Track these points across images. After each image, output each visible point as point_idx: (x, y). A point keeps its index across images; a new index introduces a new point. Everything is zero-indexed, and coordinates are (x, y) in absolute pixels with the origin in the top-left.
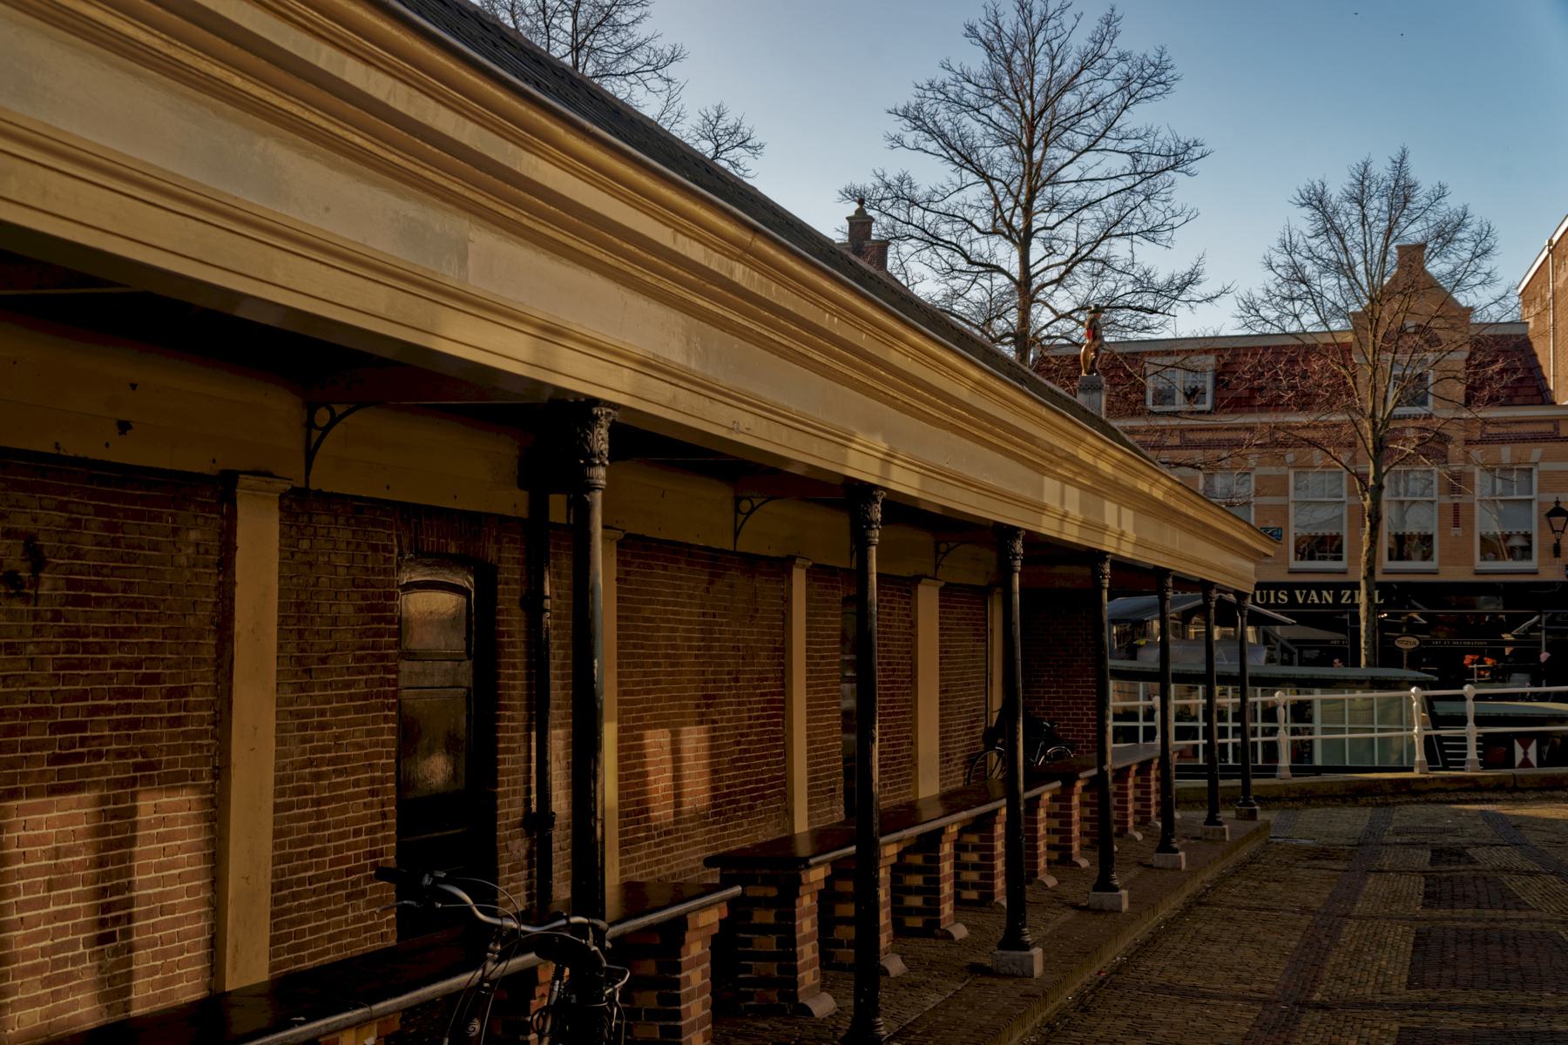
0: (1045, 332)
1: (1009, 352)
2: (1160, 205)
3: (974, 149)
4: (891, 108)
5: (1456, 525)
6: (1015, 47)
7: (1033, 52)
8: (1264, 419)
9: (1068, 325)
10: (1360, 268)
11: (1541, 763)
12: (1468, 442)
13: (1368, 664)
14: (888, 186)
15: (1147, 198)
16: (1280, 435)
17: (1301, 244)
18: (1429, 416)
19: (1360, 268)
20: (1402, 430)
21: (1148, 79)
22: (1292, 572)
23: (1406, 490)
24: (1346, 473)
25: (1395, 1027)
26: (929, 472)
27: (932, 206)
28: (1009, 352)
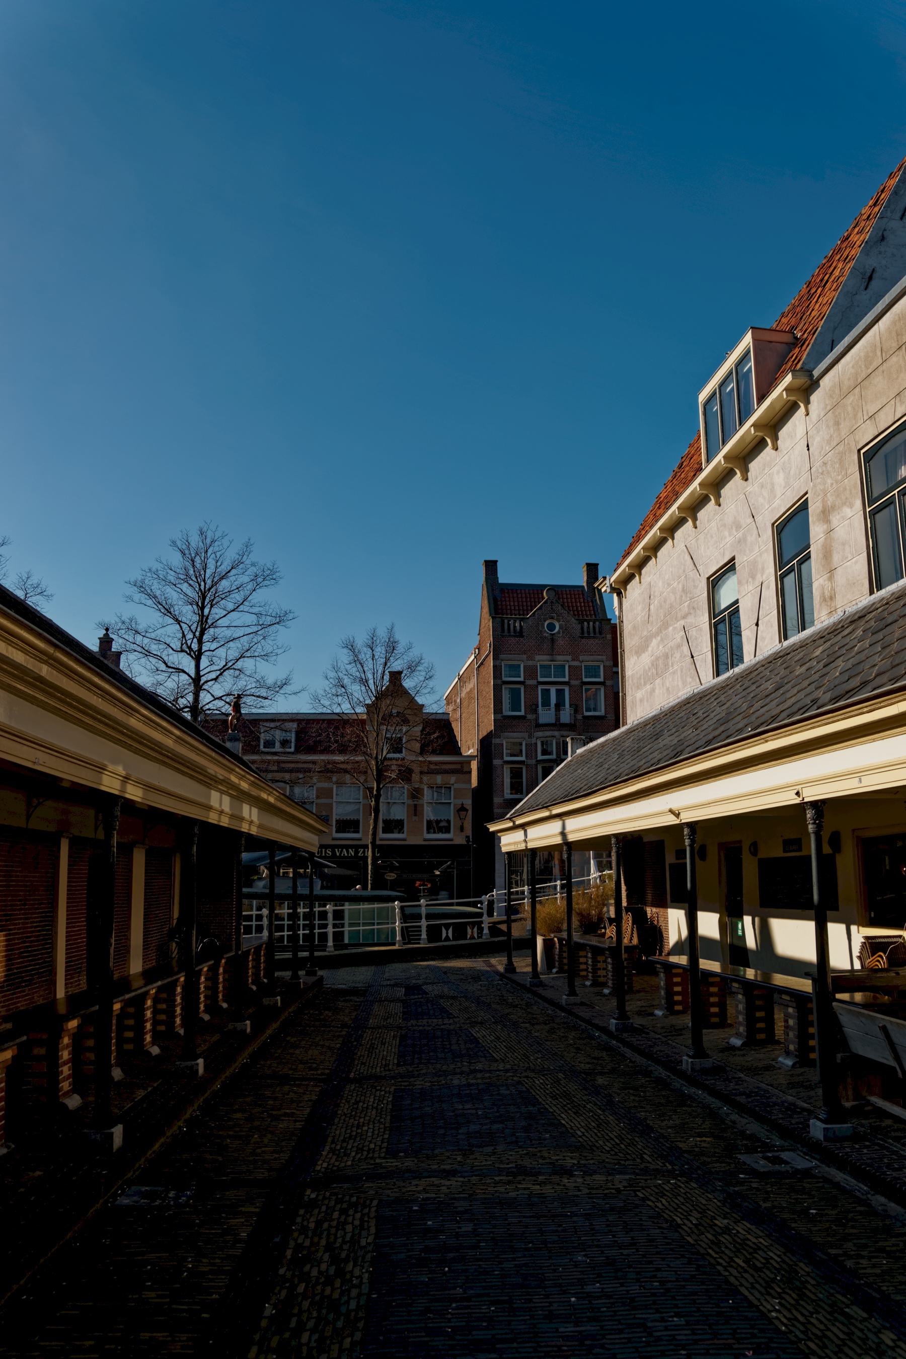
0: (207, 707)
1: (188, 716)
2: (270, 642)
3: (172, 606)
4: (127, 580)
5: (415, 815)
6: (197, 554)
7: (206, 558)
8: (322, 758)
9: (220, 703)
10: (371, 682)
11: (455, 939)
12: (421, 773)
13: (372, 889)
14: (123, 622)
15: (264, 638)
16: (330, 766)
17: (342, 667)
18: (403, 759)
19: (371, 682)
20: (390, 766)
21: (265, 577)
22: (334, 839)
23: (391, 796)
24: (362, 787)
25: (392, 1089)
26: (148, 787)
27: (147, 635)
28: (188, 716)
